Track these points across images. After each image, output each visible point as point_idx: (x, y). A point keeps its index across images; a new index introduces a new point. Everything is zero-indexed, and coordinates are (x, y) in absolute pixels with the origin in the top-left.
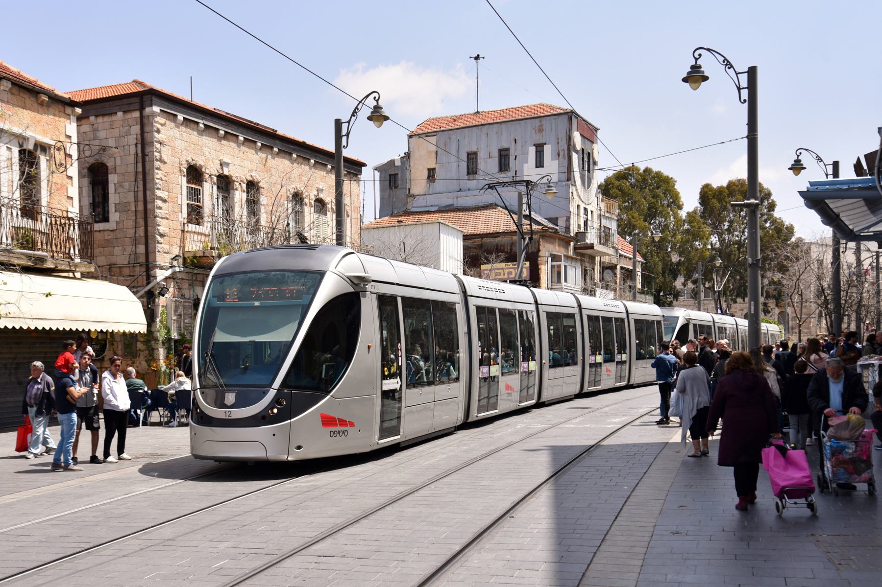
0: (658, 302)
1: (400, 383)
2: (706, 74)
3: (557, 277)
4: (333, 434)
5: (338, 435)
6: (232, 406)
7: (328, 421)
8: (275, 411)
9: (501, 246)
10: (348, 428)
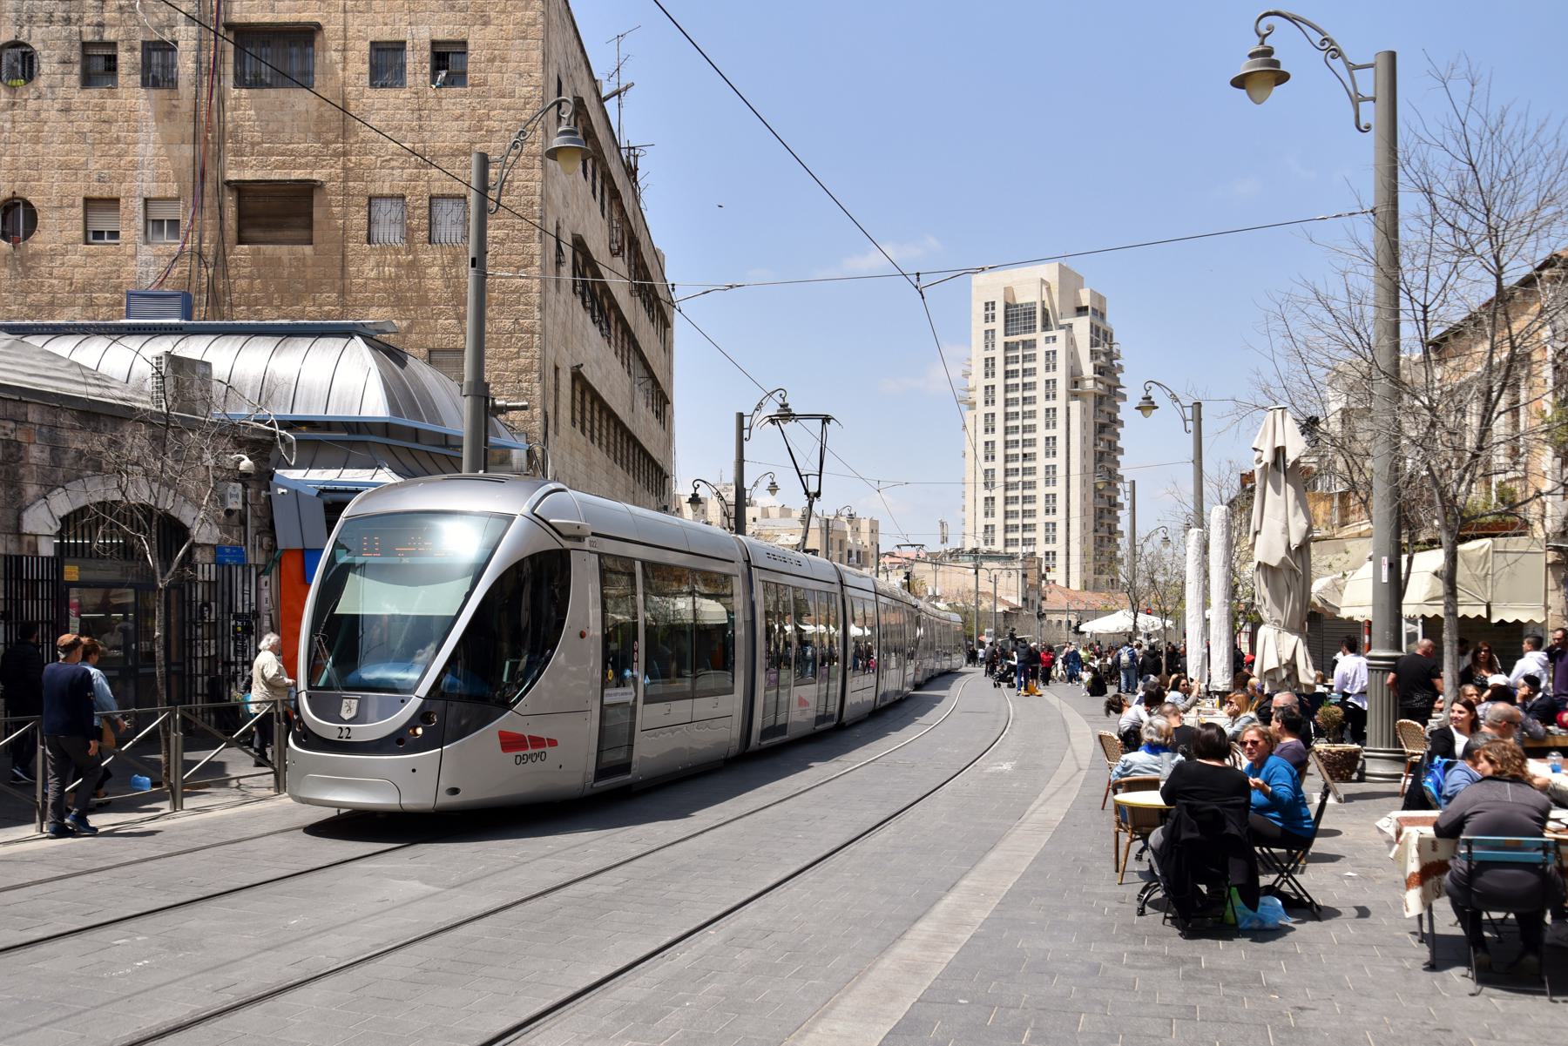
1: (634, 694)
2: (1283, 68)
3: (1107, 581)
4: (521, 760)
5: (530, 761)
6: (350, 721)
7: (510, 742)
8: (420, 731)
10: (547, 749)
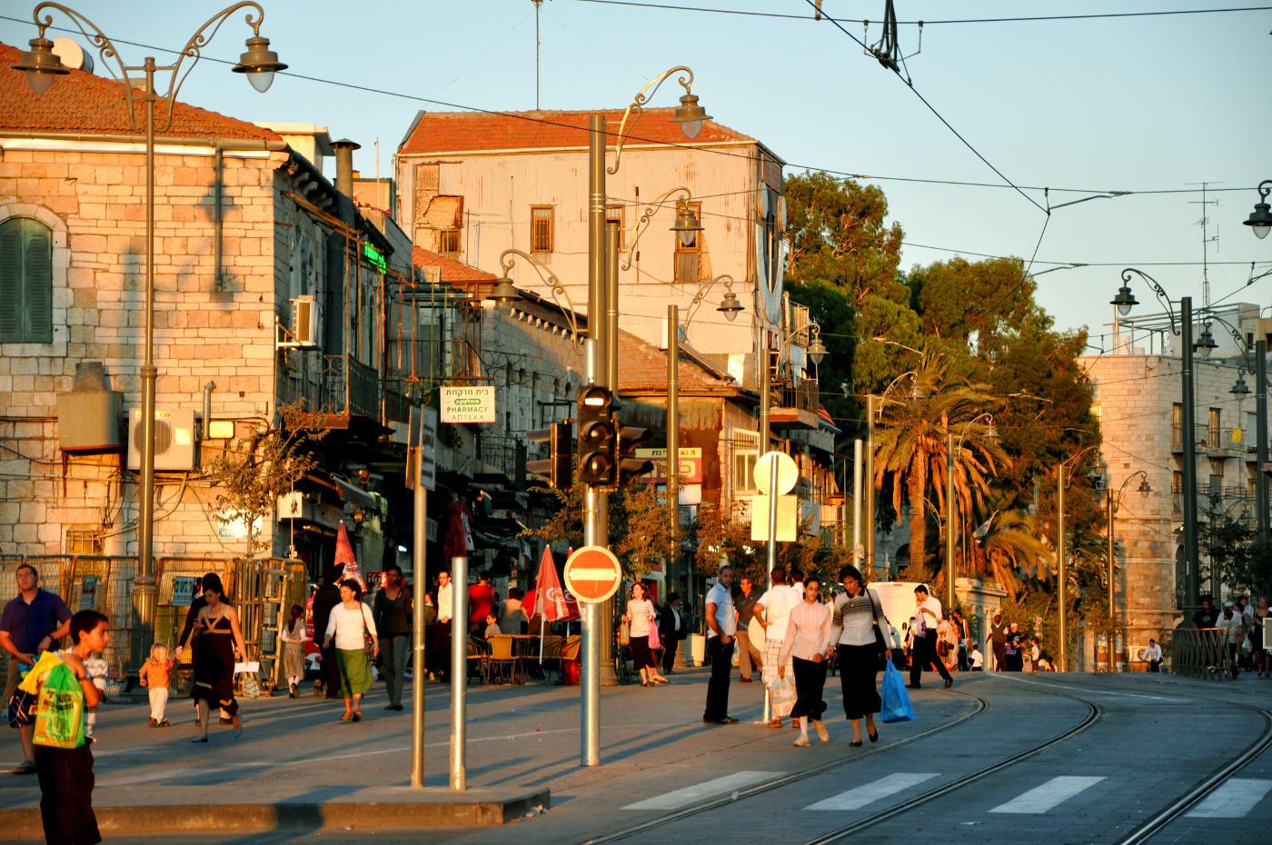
0: (69, 707)
9: (643, 414)
